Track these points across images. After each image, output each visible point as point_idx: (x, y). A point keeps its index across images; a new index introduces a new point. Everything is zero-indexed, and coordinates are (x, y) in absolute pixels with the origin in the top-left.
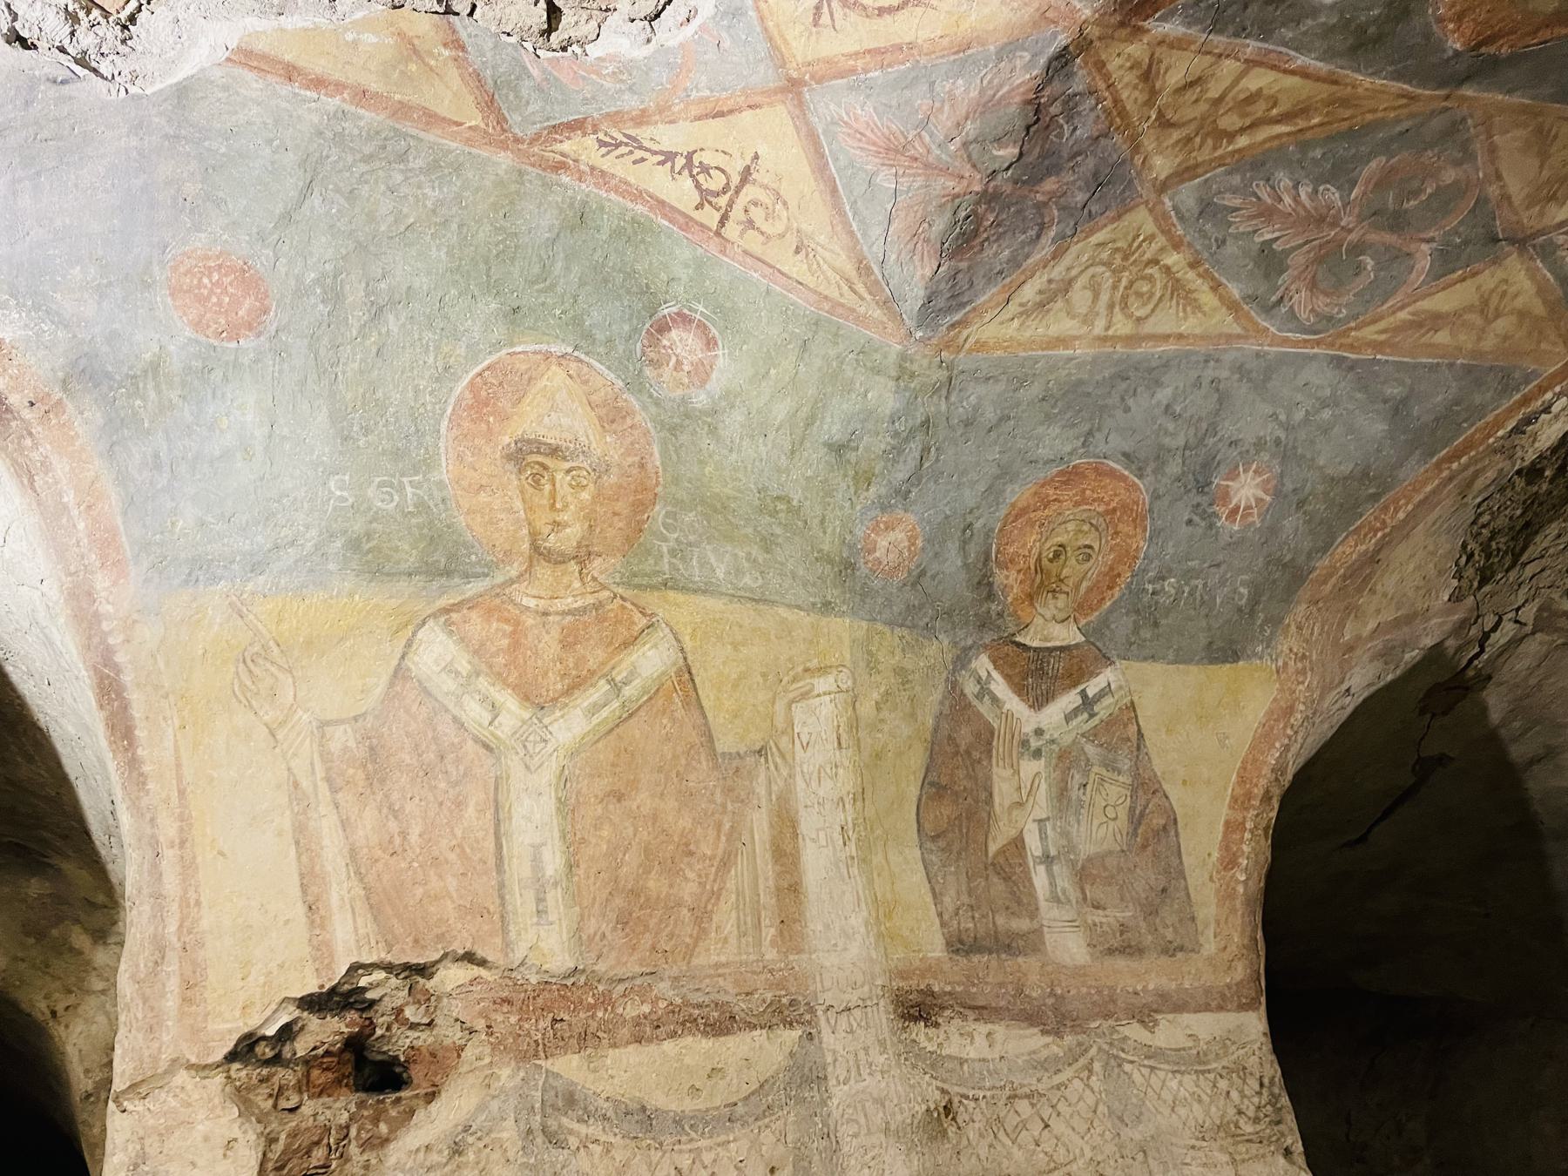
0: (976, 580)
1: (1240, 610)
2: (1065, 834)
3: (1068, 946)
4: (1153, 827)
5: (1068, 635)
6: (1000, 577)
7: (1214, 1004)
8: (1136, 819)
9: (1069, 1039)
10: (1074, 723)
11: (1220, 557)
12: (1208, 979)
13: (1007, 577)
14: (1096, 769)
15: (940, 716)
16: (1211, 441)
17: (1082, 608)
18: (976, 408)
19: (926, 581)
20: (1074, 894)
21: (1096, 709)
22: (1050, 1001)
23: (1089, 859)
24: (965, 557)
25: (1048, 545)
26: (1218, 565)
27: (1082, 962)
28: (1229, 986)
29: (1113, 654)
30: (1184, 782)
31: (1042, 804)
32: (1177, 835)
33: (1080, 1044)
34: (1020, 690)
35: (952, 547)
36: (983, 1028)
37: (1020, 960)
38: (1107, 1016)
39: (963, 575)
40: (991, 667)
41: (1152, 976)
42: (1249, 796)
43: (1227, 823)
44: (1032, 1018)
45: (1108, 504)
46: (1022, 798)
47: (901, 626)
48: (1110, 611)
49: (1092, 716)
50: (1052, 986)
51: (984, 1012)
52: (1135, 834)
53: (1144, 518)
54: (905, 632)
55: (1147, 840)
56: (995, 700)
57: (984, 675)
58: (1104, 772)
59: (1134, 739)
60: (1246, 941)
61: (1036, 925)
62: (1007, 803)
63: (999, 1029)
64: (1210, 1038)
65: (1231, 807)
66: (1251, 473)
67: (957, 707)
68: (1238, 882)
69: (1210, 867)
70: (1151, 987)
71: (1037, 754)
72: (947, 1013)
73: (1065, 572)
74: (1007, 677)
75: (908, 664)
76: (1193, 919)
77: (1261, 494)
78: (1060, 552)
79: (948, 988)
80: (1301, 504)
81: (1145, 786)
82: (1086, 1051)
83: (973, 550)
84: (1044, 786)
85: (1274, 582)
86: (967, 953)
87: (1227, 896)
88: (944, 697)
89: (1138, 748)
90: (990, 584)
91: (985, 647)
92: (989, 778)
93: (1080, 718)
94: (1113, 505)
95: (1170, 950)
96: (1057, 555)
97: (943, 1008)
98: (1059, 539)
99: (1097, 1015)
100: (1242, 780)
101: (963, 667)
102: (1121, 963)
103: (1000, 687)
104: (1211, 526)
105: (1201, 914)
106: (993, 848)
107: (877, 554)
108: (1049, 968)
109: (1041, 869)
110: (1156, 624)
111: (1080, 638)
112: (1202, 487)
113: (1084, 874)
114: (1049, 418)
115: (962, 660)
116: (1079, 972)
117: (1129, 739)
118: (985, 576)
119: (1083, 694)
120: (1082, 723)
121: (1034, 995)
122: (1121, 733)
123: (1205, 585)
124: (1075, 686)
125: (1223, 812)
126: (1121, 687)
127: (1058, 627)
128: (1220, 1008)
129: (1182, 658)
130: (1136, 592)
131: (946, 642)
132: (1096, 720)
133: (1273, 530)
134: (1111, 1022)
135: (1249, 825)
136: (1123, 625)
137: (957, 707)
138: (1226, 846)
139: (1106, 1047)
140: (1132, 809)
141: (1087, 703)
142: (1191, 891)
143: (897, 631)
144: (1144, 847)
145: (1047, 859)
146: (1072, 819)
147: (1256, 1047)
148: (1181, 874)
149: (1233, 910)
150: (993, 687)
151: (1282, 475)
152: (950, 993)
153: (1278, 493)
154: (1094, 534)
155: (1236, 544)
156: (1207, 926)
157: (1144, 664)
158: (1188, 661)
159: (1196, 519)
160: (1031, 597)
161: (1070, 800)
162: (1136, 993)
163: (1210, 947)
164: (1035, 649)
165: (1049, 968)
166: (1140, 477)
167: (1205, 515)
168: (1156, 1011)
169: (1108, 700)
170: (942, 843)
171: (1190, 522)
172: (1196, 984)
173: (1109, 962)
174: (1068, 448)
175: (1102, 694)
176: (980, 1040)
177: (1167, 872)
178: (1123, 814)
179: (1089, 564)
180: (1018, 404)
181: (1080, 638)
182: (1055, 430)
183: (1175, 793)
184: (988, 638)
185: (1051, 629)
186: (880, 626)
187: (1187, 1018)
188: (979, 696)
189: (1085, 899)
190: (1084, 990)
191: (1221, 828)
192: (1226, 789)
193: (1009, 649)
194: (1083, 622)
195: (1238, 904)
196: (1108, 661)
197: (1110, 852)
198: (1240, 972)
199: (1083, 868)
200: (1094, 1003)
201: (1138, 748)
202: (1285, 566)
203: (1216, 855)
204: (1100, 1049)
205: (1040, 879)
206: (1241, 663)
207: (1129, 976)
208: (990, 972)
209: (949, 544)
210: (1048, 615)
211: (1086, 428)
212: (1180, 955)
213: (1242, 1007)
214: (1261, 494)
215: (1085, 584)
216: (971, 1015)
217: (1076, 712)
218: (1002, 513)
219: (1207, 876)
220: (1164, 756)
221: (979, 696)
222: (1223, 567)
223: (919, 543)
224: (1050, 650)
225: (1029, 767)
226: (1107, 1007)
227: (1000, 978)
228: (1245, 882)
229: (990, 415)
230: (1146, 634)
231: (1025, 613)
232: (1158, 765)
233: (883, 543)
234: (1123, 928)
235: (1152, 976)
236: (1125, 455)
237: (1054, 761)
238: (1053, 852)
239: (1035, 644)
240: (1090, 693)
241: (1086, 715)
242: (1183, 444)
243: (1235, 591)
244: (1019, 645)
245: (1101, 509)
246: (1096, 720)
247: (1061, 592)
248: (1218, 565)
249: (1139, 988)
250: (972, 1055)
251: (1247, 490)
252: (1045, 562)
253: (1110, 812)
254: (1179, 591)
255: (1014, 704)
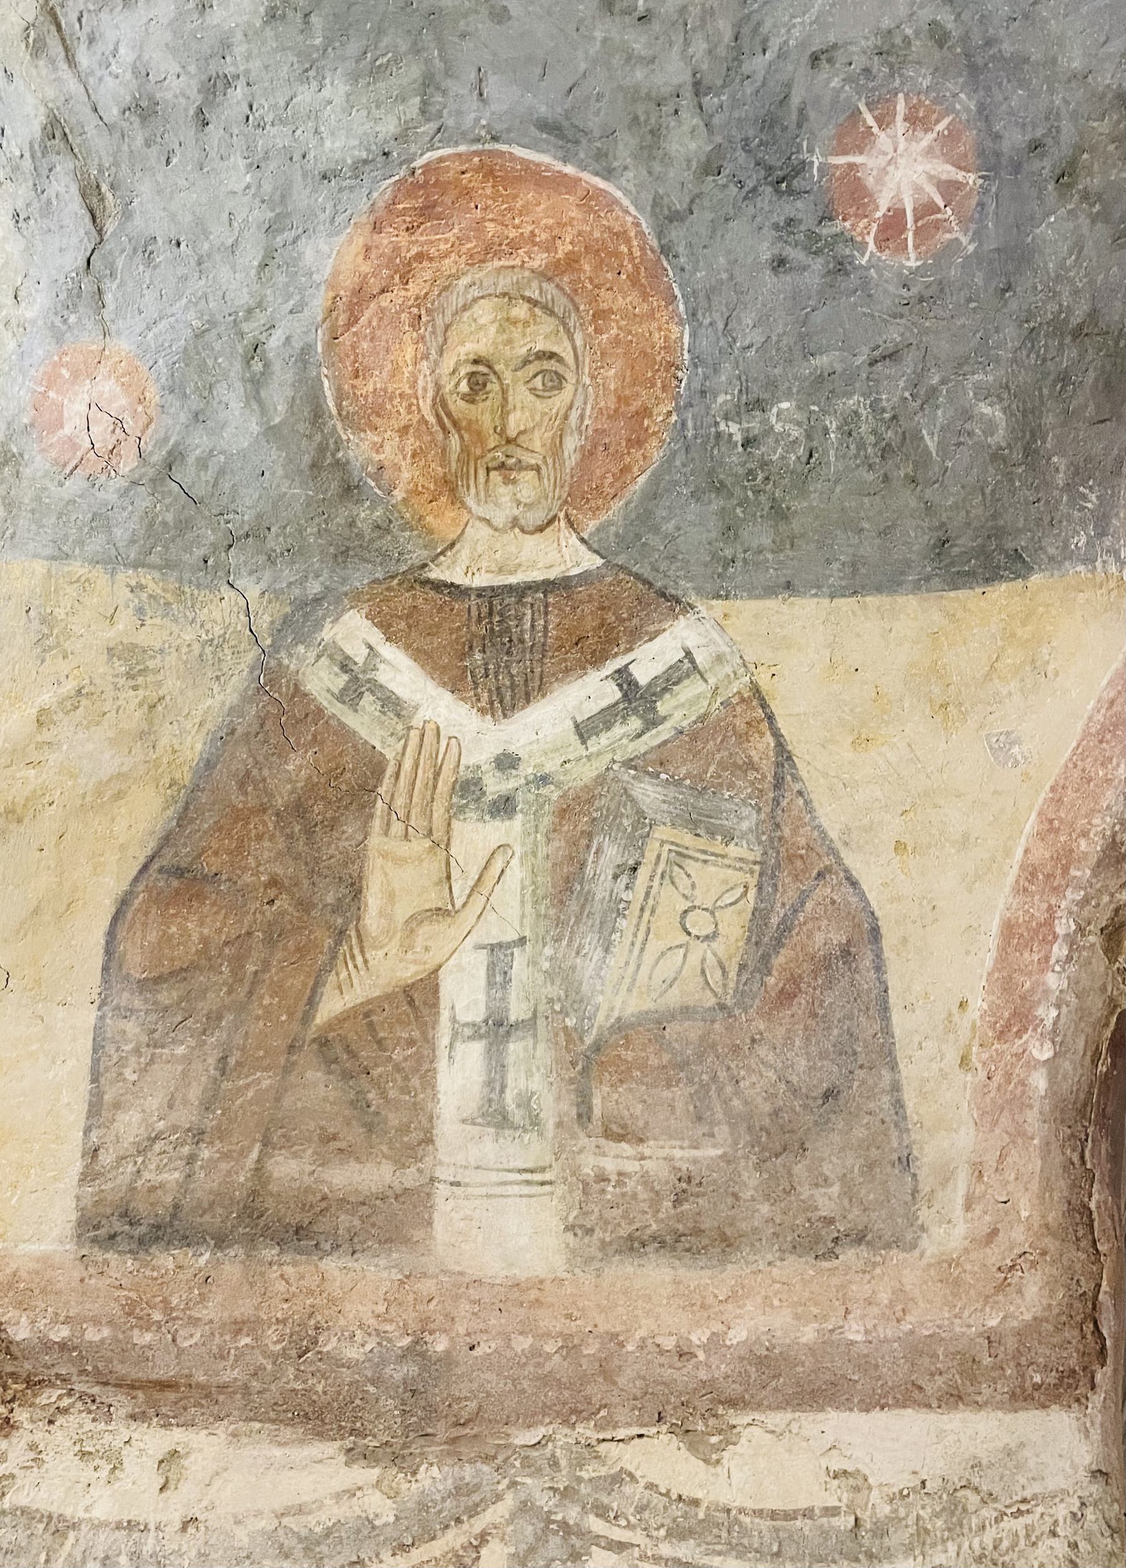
0: (307, 459)
1: (996, 456)
2: (560, 973)
3: (498, 1217)
4: (815, 958)
5: (563, 555)
6: (360, 449)
7: (931, 1388)
8: (767, 936)
9: (433, 1478)
10: (604, 739)
11: (894, 335)
12: (928, 1315)
13: (379, 448)
14: (661, 832)
15: (226, 737)
16: (758, 64)
17: (578, 497)
18: (142, 73)
19: (186, 474)
20: (552, 1105)
21: (662, 707)
22: (398, 1373)
23: (621, 1027)
24: (263, 410)
25: (448, 363)
26: (892, 356)
27: (540, 1270)
28: (991, 1339)
29: (685, 588)
30: (900, 847)
31: (509, 910)
32: (879, 967)
33: (460, 1490)
34: (457, 681)
35: (232, 398)
36: (154, 1440)
37: (331, 1265)
38: (571, 1415)
39: (273, 457)
40: (376, 637)
41: (760, 1305)
42: (1066, 859)
43: (1009, 929)
44: (321, 1413)
45: (549, 247)
46: (450, 915)
47: (136, 565)
48: (653, 494)
49: (652, 723)
50: (426, 1325)
51: (164, 1396)
52: (765, 964)
53: (657, 272)
54: (147, 578)
55: (795, 980)
56: (391, 704)
57: (359, 655)
58: (687, 839)
59: (768, 768)
60: (1054, 1216)
61: (410, 1177)
62: (402, 912)
63: (204, 1445)
64: (907, 1481)
65: (1020, 890)
66: (900, 125)
67: (279, 711)
68: (1032, 1065)
69: (964, 1034)
70: (738, 1335)
71: (504, 806)
72: (49, 1396)
73: (515, 422)
74: (421, 656)
75: (151, 636)
76: (906, 1162)
77: (948, 171)
78: (480, 376)
79: (61, 1333)
80: (1065, 177)
81: (795, 862)
82: (474, 1511)
83: (279, 397)
84: (516, 874)
85: (1064, 378)
86: (143, 1243)
87: (1001, 1101)
88: (245, 699)
89: (778, 784)
90: (341, 466)
91: (356, 598)
92: (357, 856)
93: (618, 730)
94: (564, 248)
95: (821, 1241)
96: (477, 385)
97: (34, 1384)
98: (470, 348)
99: (545, 1410)
100: (1049, 828)
101: (301, 638)
102: (656, 1274)
103: (401, 672)
104: (841, 267)
105: (930, 1152)
106: (331, 1005)
107: (67, 430)
108: (427, 1286)
109: (473, 1053)
110: (779, 513)
111: (591, 562)
112: (785, 178)
113: (592, 1061)
114: (310, 68)
115: (301, 619)
116: (524, 1294)
117: (751, 765)
118: (322, 449)
119: (623, 677)
120: (624, 739)
121: (352, 1353)
122: (739, 760)
123: (876, 408)
124: (597, 659)
125: (998, 902)
126: (719, 659)
127: (531, 541)
128: (953, 1398)
129: (858, 581)
130: (699, 445)
131: (253, 593)
132: (664, 732)
133: (1011, 260)
134: (586, 1431)
135: (1064, 926)
136: (693, 524)
137: (279, 711)
138: (1005, 978)
139: (545, 1501)
140: (759, 916)
141: (637, 699)
142: (910, 1098)
143: (128, 576)
144: (786, 997)
145: (497, 1029)
146: (590, 941)
147: (1061, 1512)
148: (887, 1056)
149: (1019, 1134)
150: (383, 676)
151: (984, 113)
152: (63, 1346)
153: (990, 163)
154: (548, 324)
155: (923, 299)
156: (946, 1178)
157: (771, 604)
158: (890, 581)
159: (795, 254)
160: (450, 488)
161: (587, 899)
162: (684, 1354)
163: (948, 1230)
164: (481, 592)
165: (427, 1286)
166: (608, 174)
167: (814, 244)
168: (732, 1403)
169: (690, 689)
170: (167, 996)
171: (780, 264)
172: (888, 1331)
173: (622, 1270)
174: (389, 127)
175: (670, 680)
176: (140, 1472)
177: (844, 1051)
178: (734, 927)
179: (566, 394)
180: (225, 47)
181: (591, 562)
182: (336, 88)
183: (874, 872)
184: (360, 577)
185: (502, 544)
186: (78, 568)
187: (835, 1423)
188: (351, 695)
189: (584, 1116)
190: (522, 1344)
191: (991, 941)
192: (1008, 853)
193: (422, 598)
194: (591, 526)
195: (1032, 1120)
196: (676, 605)
197: (686, 1012)
198: (1034, 1297)
199: (597, 1047)
200: (546, 1380)
201: (778, 784)
202: (1078, 333)
203: (978, 1004)
204: (525, 1507)
205: (459, 1075)
206: (1036, 579)
207: (659, 1305)
208: (215, 1295)
209: (221, 390)
210: (500, 519)
211: (413, 71)
212: (849, 1255)
213: (1023, 1397)
214: (948, 171)
215: (571, 443)
216: (122, 1404)
217: (606, 718)
218: (319, 303)
219: (952, 1056)
220: (843, 794)
221: (351, 695)
222: (910, 361)
223: (153, 394)
224: (521, 591)
225: (475, 837)
226: (584, 1389)
227: (245, 1308)
228: (1051, 1065)
229: (178, 87)
230: (759, 535)
231: (444, 522)
232: (831, 816)
233: (75, 409)
234: (686, 1185)
235: (760, 1305)
236: (544, 126)
237: (546, 821)
238: (517, 1011)
239: (480, 581)
240: (643, 674)
241: (635, 723)
242: (686, 77)
243: (967, 415)
244: (438, 586)
245: (540, 260)
246: (664, 732)
247: (520, 466)
248: (892, 356)
249: (699, 1337)
250: (98, 1513)
251: (904, 167)
252: (458, 406)
253: (700, 923)
254: (814, 431)
255: (437, 706)
